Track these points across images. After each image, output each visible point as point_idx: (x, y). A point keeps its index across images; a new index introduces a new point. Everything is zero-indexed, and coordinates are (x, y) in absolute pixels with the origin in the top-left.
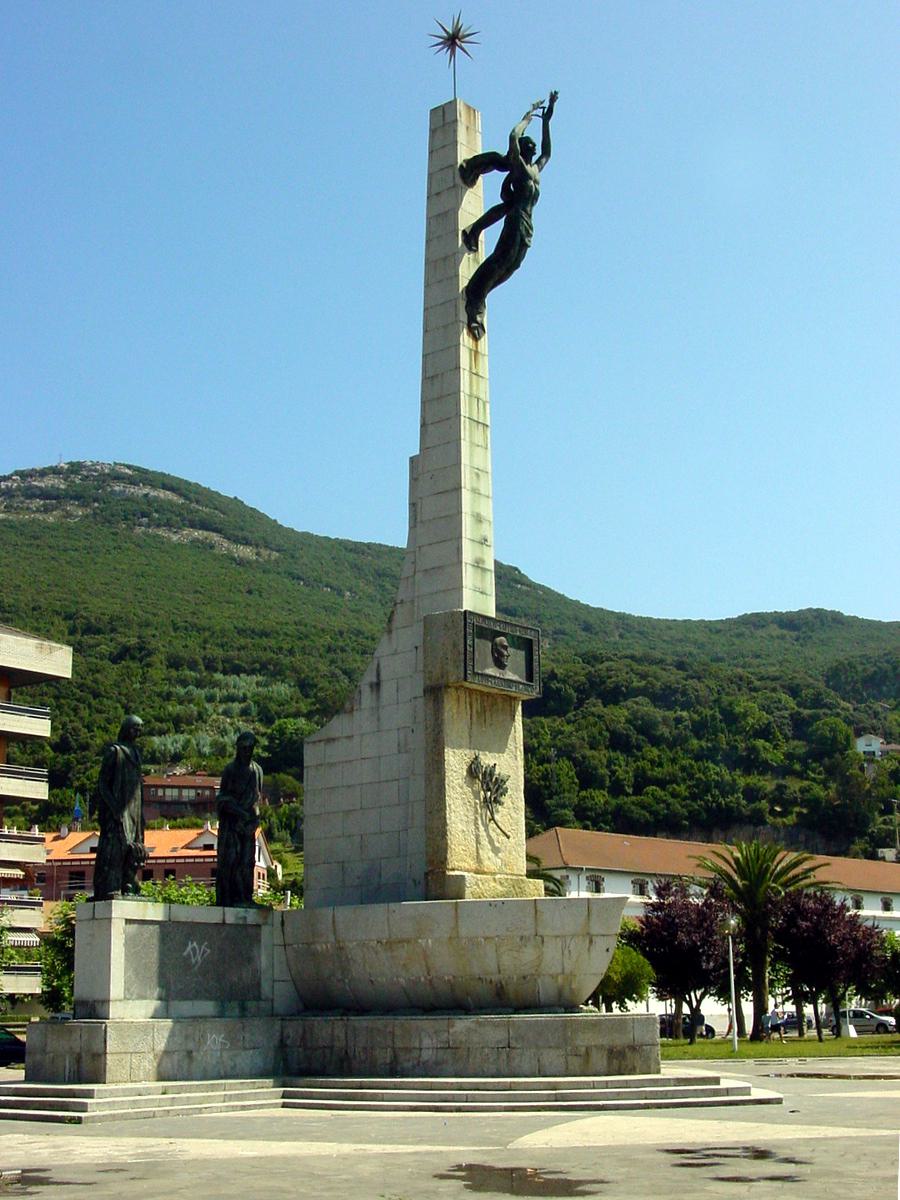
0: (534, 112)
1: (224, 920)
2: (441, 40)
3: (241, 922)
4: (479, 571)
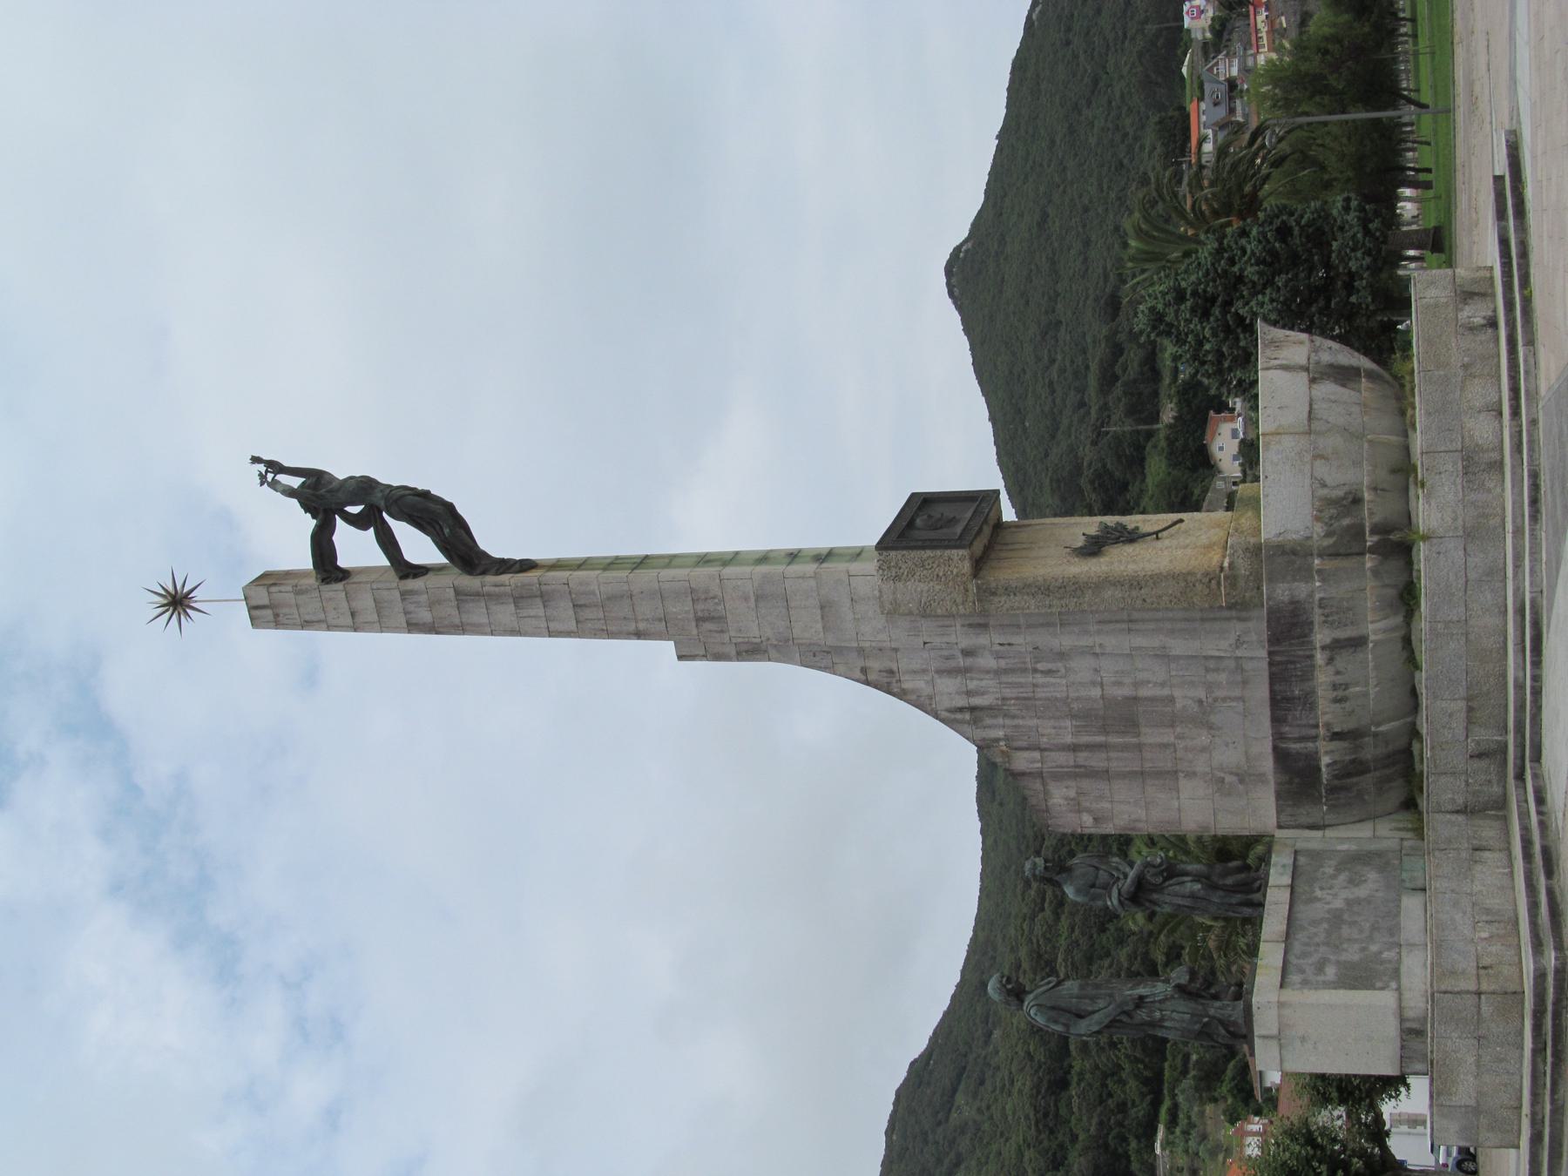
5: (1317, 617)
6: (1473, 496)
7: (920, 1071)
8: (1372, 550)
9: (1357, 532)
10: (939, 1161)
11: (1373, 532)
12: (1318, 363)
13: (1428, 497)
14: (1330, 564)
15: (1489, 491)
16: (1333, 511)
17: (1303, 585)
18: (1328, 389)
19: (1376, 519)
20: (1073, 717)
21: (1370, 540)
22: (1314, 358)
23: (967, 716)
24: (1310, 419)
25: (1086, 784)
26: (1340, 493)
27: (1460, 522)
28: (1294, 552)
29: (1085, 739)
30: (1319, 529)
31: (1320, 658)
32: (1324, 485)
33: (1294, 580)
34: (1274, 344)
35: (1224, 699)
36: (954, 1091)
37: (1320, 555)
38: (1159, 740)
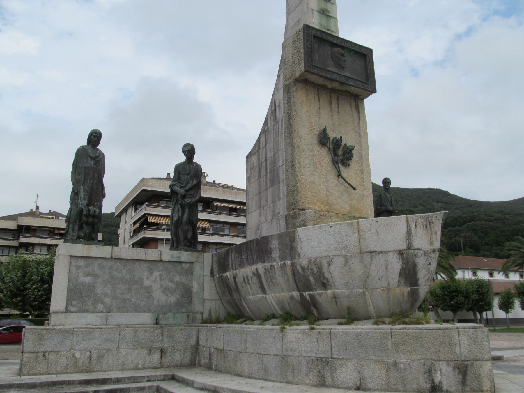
4: (325, 16)
5: (267, 265)
6: (304, 363)
7: (446, 194)
8: (301, 295)
9: (308, 287)
10: (424, 201)
11: (310, 295)
12: (415, 255)
13: (303, 332)
14: (289, 270)
15: (307, 375)
16: (315, 271)
17: (278, 255)
18: (396, 265)
19: (318, 297)
20: (274, 155)
21: (306, 294)
22: (420, 253)
23: (273, 109)
24: (371, 252)
25: (257, 169)
26: (326, 275)
27: (290, 353)
28: (292, 248)
29: (268, 163)
30: (305, 263)
31: (254, 268)
32: (329, 264)
33: (280, 250)
34: (428, 225)
35: (280, 225)
36: (442, 202)
37: (292, 265)
38: (269, 197)
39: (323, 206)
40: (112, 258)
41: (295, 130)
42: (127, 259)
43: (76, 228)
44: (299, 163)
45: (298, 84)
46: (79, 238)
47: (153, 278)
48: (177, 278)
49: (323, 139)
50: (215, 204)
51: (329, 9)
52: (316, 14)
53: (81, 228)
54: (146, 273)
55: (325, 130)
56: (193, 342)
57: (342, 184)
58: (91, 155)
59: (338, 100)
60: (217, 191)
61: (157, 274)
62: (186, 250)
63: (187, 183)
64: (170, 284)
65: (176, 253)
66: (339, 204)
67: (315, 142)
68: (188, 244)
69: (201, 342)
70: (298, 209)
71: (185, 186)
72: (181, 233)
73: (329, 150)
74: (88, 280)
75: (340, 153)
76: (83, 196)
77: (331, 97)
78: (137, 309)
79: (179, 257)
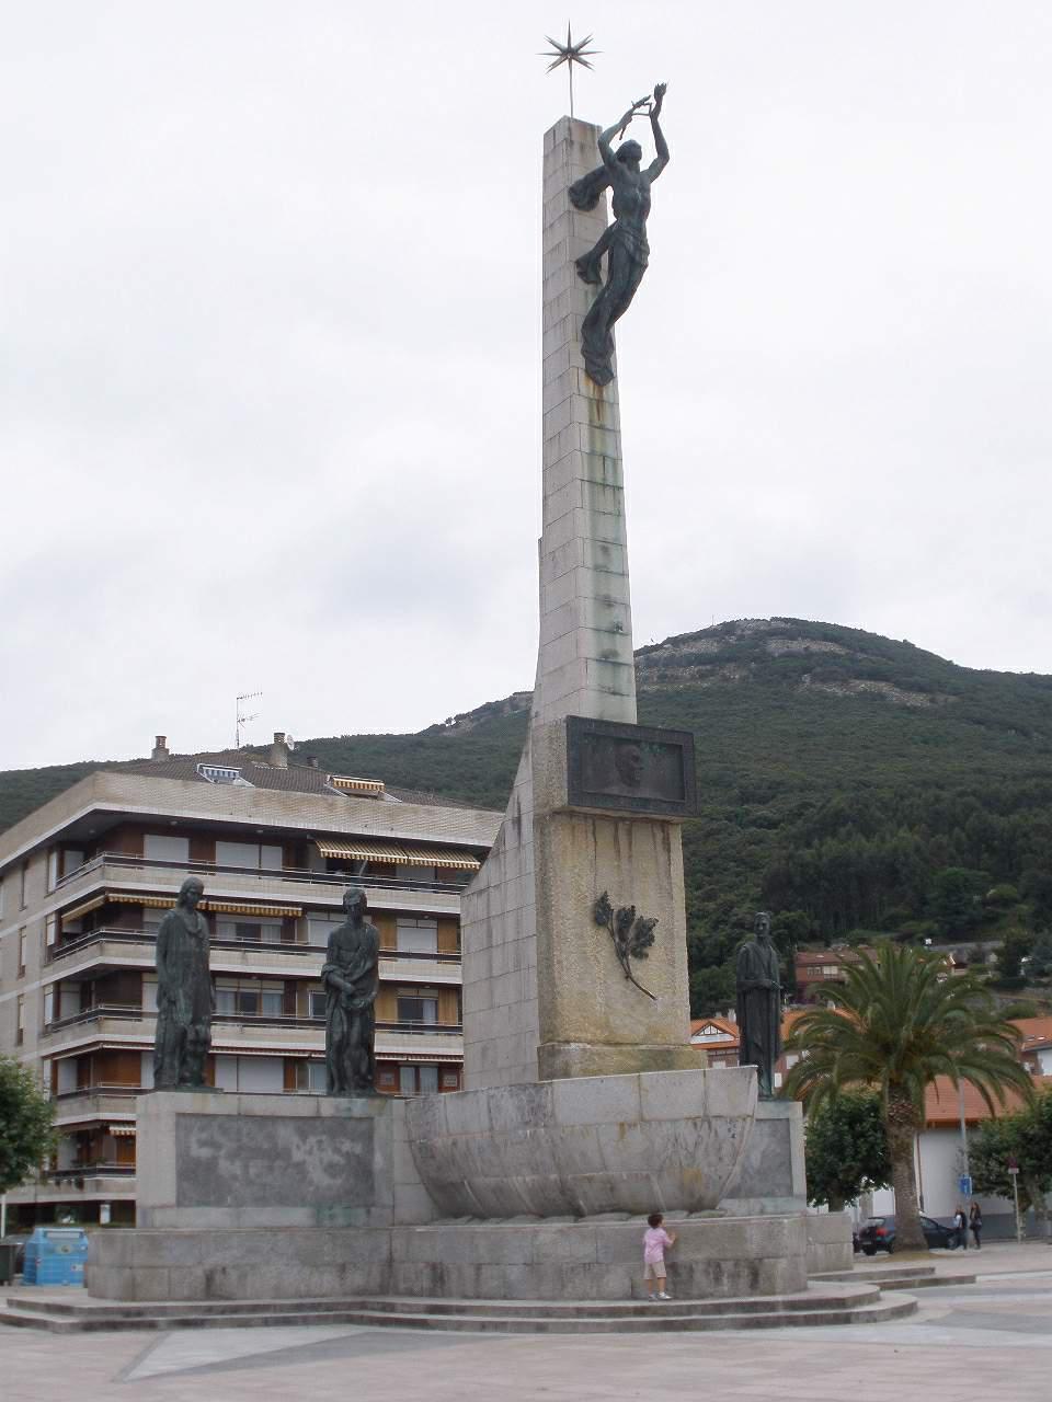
0: (637, 111)
1: (318, 1111)
2: (583, 57)
3: (344, 1114)
4: (610, 666)
39: (599, 1031)
40: (239, 1114)
41: (553, 906)
42: (261, 1116)
43: (176, 1063)
44: (559, 962)
45: (557, 817)
46: (183, 1080)
47: (307, 1147)
48: (347, 1146)
49: (601, 913)
50: (328, 850)
51: (620, 650)
52: (593, 666)
53: (183, 1062)
54: (296, 1140)
55: (604, 898)
56: (384, 1254)
57: (634, 990)
58: (190, 928)
59: (629, 833)
60: (331, 807)
61: (312, 1140)
62: (359, 1096)
63: (356, 967)
64: (337, 1158)
65: (343, 1102)
66: (626, 1026)
67: (588, 920)
68: (362, 1083)
69: (396, 1256)
70: (559, 1042)
71: (350, 975)
72: (347, 1063)
73: (612, 934)
74: (205, 1153)
75: (631, 934)
76: (183, 1007)
77: (616, 830)
78: (283, 1200)
79: (349, 1109)
